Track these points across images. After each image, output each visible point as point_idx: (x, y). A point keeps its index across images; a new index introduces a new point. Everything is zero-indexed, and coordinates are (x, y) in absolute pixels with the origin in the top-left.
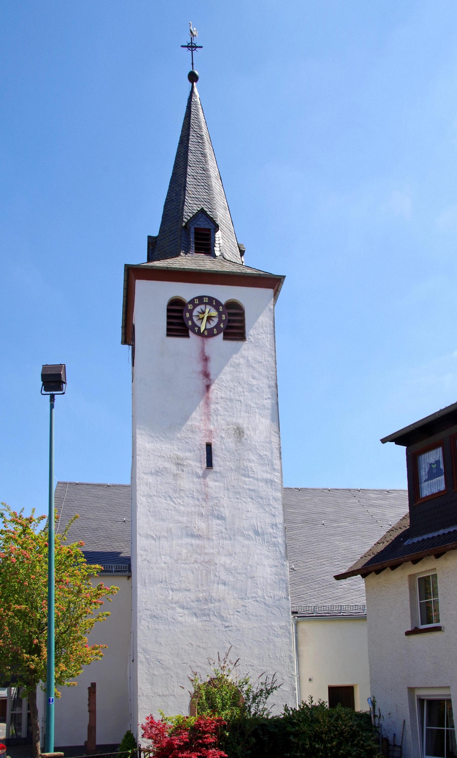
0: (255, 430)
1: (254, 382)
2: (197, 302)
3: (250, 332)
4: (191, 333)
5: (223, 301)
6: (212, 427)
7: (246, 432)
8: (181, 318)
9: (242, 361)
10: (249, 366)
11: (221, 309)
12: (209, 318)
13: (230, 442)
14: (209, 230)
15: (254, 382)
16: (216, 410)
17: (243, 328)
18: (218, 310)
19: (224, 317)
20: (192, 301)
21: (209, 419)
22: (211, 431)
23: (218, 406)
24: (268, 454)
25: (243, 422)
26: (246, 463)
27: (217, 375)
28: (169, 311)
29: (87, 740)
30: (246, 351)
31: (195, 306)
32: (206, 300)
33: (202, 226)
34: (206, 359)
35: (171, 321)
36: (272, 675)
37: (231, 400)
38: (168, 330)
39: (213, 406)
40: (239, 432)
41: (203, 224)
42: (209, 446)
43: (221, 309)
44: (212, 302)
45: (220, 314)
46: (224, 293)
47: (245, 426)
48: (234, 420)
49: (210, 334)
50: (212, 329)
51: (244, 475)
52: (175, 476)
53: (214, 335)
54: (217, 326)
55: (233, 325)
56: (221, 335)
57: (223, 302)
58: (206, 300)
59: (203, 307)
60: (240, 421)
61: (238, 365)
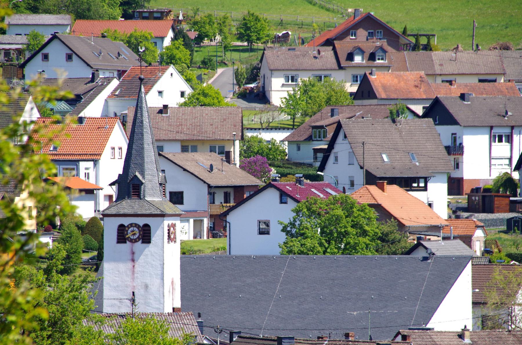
0: (153, 285)
1: (154, 263)
2: (130, 226)
3: (153, 239)
4: (127, 242)
5: (141, 225)
6: (135, 285)
7: (149, 286)
8: (123, 233)
9: (149, 253)
10: (152, 255)
11: (140, 229)
12: (134, 234)
13: (142, 291)
14: (139, 185)
15: (154, 263)
16: (137, 277)
17: (150, 239)
18: (138, 229)
19: (141, 233)
20: (128, 226)
21: (134, 281)
22: (134, 286)
23: (138, 275)
24: (158, 296)
25: (148, 282)
26: (149, 301)
27: (137, 261)
28: (118, 230)
29: (436, 330)
30: (150, 248)
31: (129, 228)
32: (134, 225)
33: (136, 183)
34: (133, 253)
35: (119, 238)
36: (435, 71)
37: (143, 272)
38: (118, 239)
39: (136, 275)
40: (146, 287)
41: (136, 183)
42: (133, 293)
43: (140, 229)
44: (137, 225)
45: (140, 231)
46: (141, 221)
47: (149, 283)
48: (145, 281)
49: (136, 241)
50: (136, 239)
51: (148, 306)
52: (119, 307)
53: (137, 242)
54: (138, 237)
55: (146, 235)
56: (141, 241)
57: (141, 225)
58: (134, 225)
59: (132, 237)
60: (147, 281)
61: (147, 255)
